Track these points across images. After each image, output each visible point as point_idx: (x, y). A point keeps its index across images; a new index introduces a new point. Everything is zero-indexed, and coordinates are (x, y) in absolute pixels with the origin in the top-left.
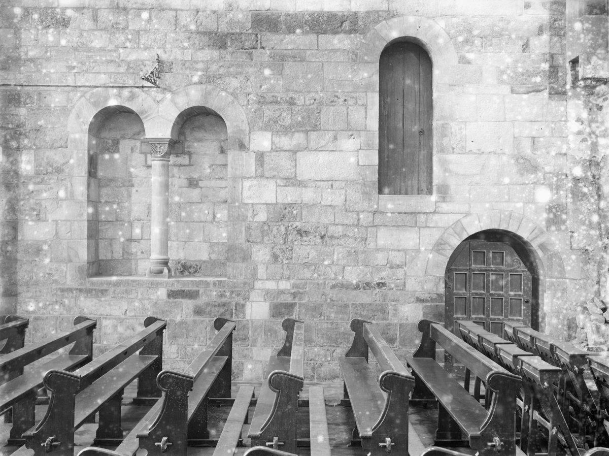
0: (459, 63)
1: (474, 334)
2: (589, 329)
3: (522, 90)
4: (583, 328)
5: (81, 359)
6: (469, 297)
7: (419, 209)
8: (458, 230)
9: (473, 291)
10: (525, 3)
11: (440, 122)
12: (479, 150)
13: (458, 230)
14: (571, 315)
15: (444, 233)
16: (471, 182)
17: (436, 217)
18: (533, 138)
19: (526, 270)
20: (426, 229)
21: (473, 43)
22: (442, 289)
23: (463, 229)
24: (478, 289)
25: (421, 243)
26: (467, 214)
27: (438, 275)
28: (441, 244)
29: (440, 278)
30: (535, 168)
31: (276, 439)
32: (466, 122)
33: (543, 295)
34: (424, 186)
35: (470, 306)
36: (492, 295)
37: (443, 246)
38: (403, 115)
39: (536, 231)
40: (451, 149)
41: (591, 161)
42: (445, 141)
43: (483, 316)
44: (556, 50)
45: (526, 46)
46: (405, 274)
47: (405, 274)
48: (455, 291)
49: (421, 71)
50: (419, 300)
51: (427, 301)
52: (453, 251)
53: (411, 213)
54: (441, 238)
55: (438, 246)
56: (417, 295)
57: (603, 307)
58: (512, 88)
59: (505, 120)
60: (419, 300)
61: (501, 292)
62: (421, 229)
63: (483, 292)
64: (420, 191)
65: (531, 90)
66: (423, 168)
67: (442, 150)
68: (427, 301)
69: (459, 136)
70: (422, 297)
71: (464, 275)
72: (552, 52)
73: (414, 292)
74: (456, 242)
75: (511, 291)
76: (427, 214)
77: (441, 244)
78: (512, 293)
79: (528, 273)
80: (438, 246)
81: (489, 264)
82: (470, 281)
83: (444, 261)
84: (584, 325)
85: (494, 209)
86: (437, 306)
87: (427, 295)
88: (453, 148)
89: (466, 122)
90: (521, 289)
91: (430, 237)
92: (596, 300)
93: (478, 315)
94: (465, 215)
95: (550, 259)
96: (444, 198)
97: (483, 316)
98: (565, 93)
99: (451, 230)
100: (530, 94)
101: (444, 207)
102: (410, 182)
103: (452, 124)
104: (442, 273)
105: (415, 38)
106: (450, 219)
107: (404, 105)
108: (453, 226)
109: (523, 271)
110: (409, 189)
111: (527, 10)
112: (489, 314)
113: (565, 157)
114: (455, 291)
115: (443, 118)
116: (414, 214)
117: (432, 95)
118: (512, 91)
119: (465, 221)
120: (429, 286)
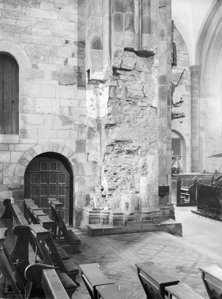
0: (32, 68)
1: (54, 204)
2: (94, 200)
3: (65, 83)
4: (92, 199)
5: (11, 275)
6: (39, 187)
7: (11, 142)
8: (31, 152)
9: (41, 183)
10: (66, 41)
11: (22, 97)
12: (42, 112)
13: (31, 152)
14: (87, 192)
15: (24, 154)
16: (38, 128)
17: (20, 146)
18: (70, 107)
19: (67, 172)
20: (14, 152)
21: (39, 58)
22: (23, 183)
23: (34, 152)
24: (44, 182)
25: (11, 159)
26: (37, 144)
27: (21, 176)
28: (22, 160)
29: (22, 177)
30: (71, 122)
31: (20, 291)
32: (36, 98)
33: (75, 184)
34: (14, 130)
35: (39, 191)
36: (50, 185)
37: (23, 161)
38: (3, 92)
39: (71, 153)
40: (27, 111)
41: (97, 119)
42: (25, 107)
43: (46, 196)
44: (81, 65)
45: (66, 62)
46: (3, 175)
47: (3, 175)
48: (31, 184)
49: (13, 70)
50: (10, 189)
51: (15, 189)
52: (29, 163)
53: (6, 144)
54: (22, 157)
55: (21, 160)
56: (9, 186)
57: (102, 188)
58: (59, 82)
59: (56, 98)
60: (10, 189)
61: (55, 183)
62: (12, 152)
63: (46, 183)
64: (12, 133)
65: (69, 84)
66: (14, 120)
67: (23, 112)
68: (15, 189)
69: (32, 105)
70: (12, 187)
71: (36, 175)
72: (79, 66)
73: (7, 184)
74: (30, 159)
75: (60, 182)
76: (15, 144)
77: (22, 160)
78: (61, 183)
79: (68, 173)
80: (21, 161)
81: (49, 170)
82: (39, 178)
83: (24, 168)
84: (93, 198)
85: (50, 142)
86: (20, 191)
87: (15, 186)
88: (29, 111)
89: (36, 98)
90: (56, 182)
91: (16, 156)
92: (99, 185)
93: (44, 195)
94: (35, 145)
95: (78, 166)
96: (24, 136)
97: (46, 196)
98: (85, 86)
99: (27, 153)
100: (68, 86)
101: (24, 141)
102: (6, 128)
103: (28, 98)
104: (23, 174)
105: (8, 53)
106: (28, 147)
107: (3, 87)
108: (29, 151)
109: (65, 173)
110: (6, 131)
111: (67, 44)
112: (49, 194)
113: (85, 117)
114: (31, 184)
115: (23, 95)
116: (8, 144)
117: (18, 83)
118: (59, 84)
119: (35, 148)
120: (16, 181)
